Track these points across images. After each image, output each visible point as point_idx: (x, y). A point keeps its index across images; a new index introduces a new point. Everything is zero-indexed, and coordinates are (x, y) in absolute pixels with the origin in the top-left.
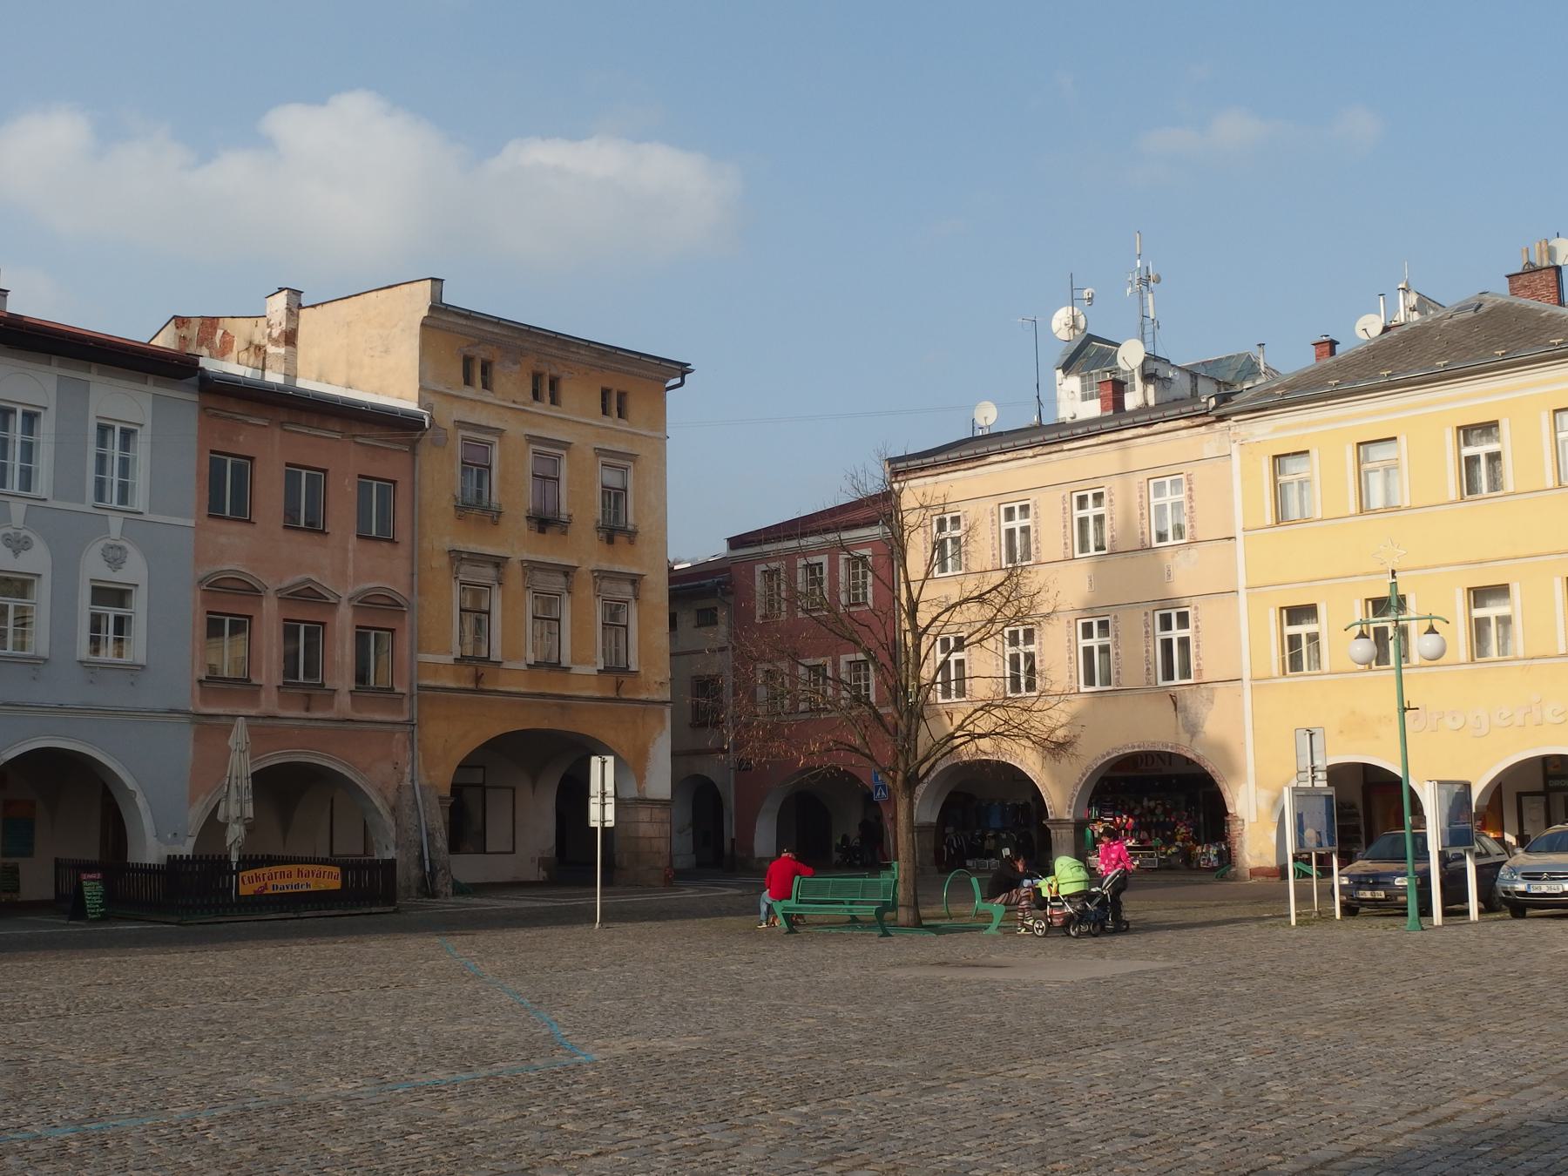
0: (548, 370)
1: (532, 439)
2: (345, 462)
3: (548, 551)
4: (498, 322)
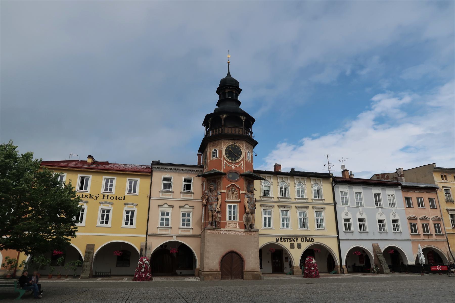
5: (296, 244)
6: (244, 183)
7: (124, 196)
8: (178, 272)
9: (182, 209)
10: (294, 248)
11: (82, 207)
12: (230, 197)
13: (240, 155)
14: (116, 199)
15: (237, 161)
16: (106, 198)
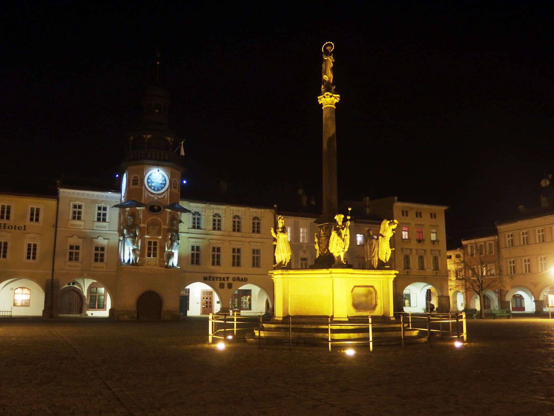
5: (226, 283)
7: (25, 226)
10: (223, 288)
11: (380, 237)
14: (15, 229)
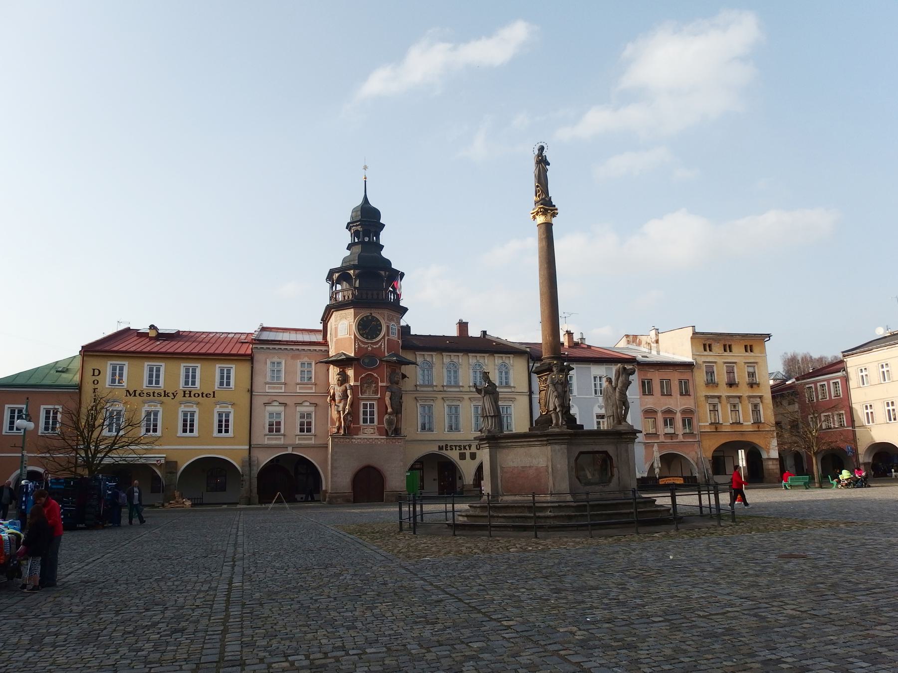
0: (728, 343)
1: (725, 363)
2: (675, 377)
3: (733, 392)
4: (711, 334)
5: (468, 453)
6: (386, 371)
8: (298, 497)
9: (299, 409)
12: (365, 392)
13: (380, 331)
15: (374, 341)
16: (187, 395)
